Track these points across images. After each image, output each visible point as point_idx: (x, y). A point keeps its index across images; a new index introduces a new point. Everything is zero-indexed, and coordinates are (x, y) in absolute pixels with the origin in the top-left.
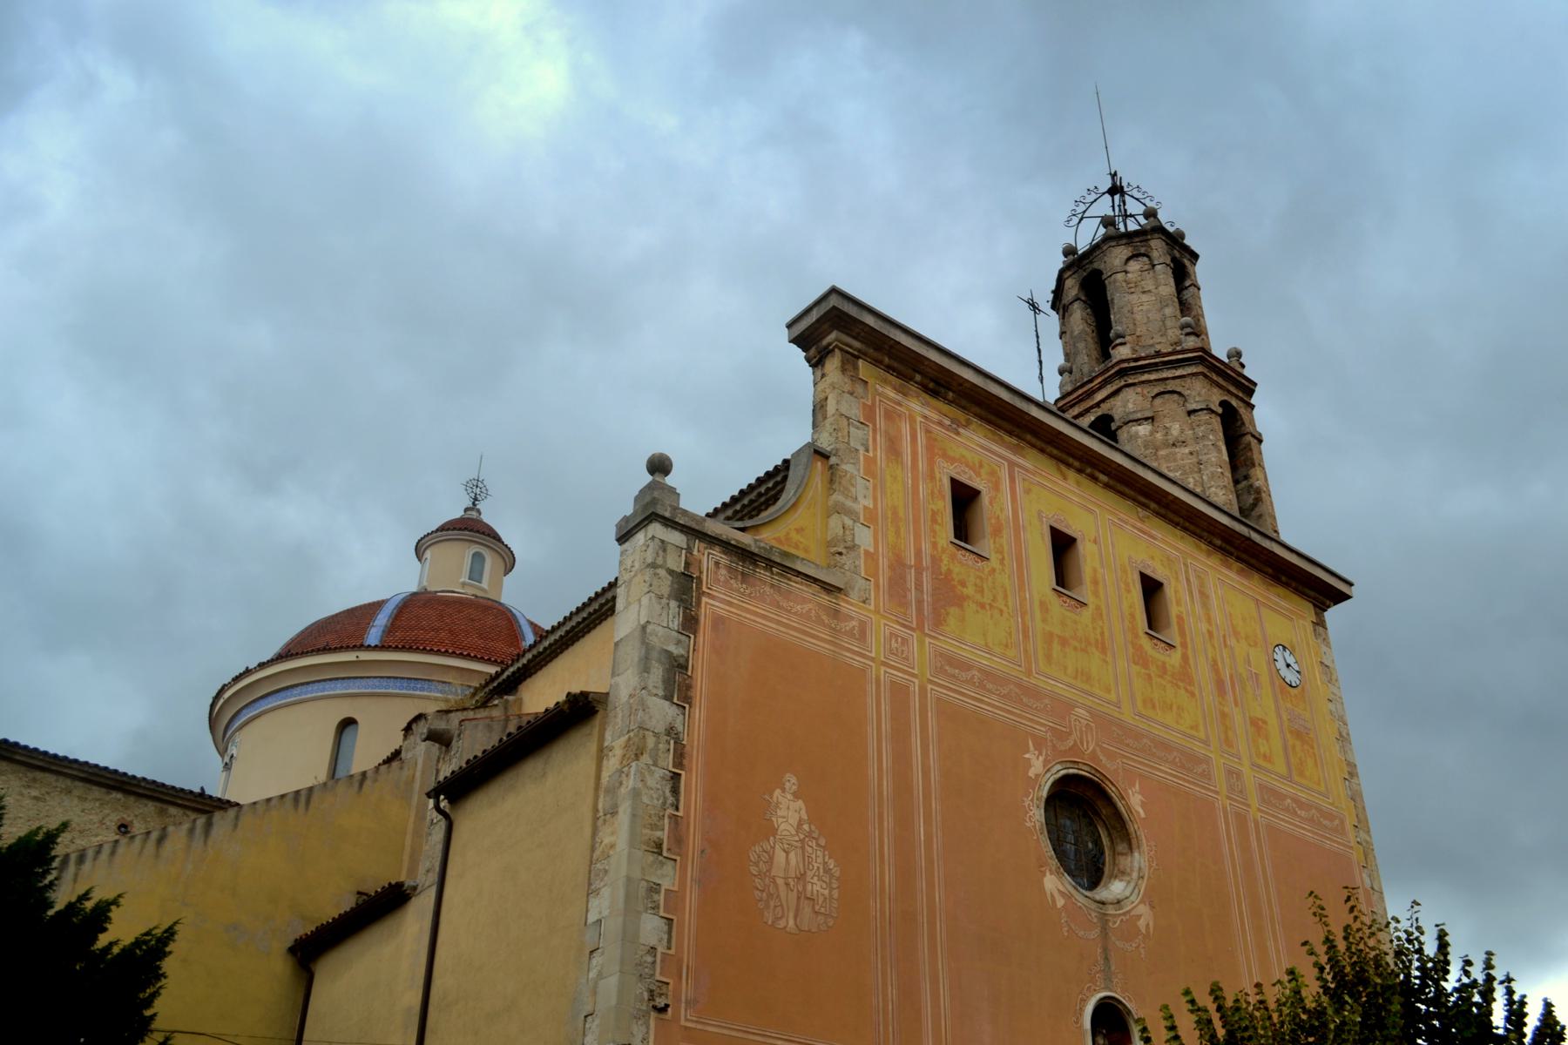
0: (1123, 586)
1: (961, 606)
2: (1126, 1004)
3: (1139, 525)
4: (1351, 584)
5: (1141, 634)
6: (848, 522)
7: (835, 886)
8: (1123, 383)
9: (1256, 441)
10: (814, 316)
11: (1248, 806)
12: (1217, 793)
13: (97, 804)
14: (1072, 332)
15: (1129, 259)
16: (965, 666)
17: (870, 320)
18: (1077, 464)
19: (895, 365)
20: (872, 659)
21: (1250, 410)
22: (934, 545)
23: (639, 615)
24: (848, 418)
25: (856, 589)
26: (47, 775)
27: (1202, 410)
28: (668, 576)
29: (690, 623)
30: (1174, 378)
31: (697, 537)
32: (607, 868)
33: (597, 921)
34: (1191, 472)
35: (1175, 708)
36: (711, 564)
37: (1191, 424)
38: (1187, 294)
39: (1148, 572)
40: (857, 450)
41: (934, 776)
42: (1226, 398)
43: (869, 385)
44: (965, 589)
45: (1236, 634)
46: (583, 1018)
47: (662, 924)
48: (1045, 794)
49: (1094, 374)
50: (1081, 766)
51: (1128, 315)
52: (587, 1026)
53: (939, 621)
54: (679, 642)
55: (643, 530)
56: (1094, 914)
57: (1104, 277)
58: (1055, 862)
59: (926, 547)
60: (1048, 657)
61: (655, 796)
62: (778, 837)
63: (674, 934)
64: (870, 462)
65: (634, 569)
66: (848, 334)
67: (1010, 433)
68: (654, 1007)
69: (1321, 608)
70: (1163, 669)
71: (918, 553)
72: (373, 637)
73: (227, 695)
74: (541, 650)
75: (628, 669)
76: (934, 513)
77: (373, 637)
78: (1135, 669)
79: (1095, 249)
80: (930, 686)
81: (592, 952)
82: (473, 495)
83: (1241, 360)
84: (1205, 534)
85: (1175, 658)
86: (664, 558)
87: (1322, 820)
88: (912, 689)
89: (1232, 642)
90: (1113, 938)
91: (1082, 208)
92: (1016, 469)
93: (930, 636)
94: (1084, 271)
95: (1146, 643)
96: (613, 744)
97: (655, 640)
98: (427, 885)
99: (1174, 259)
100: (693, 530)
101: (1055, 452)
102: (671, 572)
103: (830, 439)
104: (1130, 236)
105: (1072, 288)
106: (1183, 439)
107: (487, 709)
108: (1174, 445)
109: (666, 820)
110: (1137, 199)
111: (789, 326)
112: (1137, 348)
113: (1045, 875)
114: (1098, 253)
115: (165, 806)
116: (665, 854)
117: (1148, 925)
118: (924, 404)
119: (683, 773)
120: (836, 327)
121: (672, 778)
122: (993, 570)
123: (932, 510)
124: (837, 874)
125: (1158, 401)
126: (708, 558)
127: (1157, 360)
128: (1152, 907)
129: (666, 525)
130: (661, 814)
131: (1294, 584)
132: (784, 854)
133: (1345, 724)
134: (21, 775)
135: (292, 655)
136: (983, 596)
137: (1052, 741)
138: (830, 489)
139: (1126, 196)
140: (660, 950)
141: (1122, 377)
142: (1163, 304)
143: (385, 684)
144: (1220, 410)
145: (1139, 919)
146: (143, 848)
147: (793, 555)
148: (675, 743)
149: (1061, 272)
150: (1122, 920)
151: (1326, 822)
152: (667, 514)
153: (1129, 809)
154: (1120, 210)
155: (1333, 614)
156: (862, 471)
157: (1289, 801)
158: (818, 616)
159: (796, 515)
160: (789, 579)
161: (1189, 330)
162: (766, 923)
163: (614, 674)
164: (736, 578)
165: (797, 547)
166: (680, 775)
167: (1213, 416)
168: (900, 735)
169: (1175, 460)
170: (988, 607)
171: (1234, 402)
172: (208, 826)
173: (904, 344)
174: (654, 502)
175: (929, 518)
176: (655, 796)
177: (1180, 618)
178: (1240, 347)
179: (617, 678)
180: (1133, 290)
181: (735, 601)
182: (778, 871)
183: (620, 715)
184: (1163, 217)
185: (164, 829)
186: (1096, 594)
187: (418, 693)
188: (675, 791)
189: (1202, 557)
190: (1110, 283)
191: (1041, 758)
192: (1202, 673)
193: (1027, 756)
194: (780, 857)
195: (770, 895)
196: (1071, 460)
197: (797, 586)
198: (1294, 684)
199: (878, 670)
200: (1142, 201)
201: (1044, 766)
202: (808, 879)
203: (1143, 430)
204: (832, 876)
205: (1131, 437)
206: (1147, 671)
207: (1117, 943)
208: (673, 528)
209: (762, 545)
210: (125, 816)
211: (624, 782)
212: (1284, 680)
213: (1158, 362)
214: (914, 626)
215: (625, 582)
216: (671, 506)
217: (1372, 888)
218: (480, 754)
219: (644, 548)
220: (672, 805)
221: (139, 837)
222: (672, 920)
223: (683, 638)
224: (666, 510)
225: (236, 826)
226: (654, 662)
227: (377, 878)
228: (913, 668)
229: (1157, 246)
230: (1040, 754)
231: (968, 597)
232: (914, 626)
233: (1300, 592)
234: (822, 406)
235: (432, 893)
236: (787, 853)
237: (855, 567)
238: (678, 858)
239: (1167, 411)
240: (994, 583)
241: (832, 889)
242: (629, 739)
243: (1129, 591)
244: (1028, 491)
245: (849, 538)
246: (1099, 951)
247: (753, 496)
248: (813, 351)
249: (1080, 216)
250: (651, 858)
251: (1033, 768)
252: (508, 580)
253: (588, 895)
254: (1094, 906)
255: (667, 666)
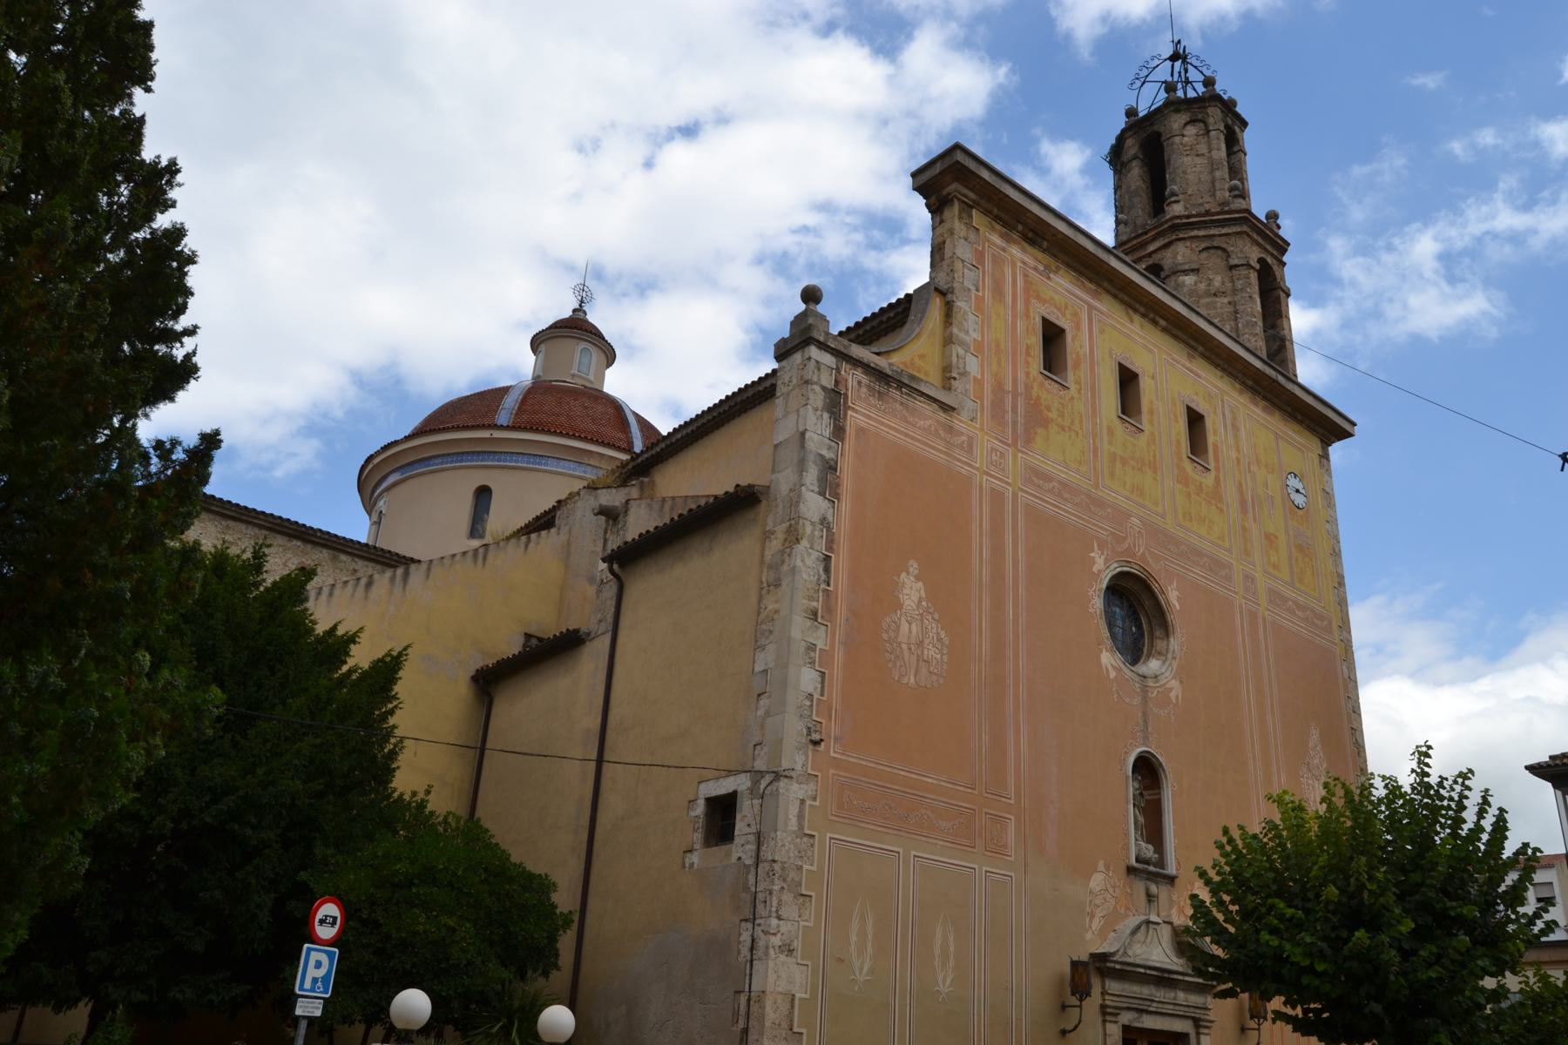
0: (1172, 417)
1: (1046, 427)
2: (1159, 758)
3: (1188, 365)
4: (1354, 424)
5: (1184, 457)
6: (961, 352)
7: (945, 652)
8: (1174, 237)
9: (1284, 295)
10: (938, 168)
11: (1259, 605)
12: (1236, 593)
13: (281, 549)
14: (1129, 187)
15: (1186, 124)
16: (1047, 478)
17: (985, 175)
18: (1142, 309)
19: (1003, 215)
20: (977, 469)
21: (1281, 267)
22: (1028, 374)
23: (797, 423)
24: (963, 261)
25: (966, 408)
26: (238, 523)
27: (1242, 265)
28: (821, 391)
29: (839, 432)
30: (1220, 235)
31: (844, 359)
32: (772, 629)
33: (764, 671)
34: (1229, 320)
35: (1207, 522)
36: (855, 383)
37: (1232, 277)
38: (1234, 159)
39: (1193, 406)
40: (969, 290)
41: (1022, 566)
42: (1263, 255)
43: (981, 232)
44: (1049, 414)
45: (1258, 462)
46: (752, 746)
47: (815, 675)
48: (1104, 586)
49: (1148, 227)
50: (1134, 566)
51: (1182, 175)
52: (756, 753)
53: (1029, 440)
54: (830, 448)
55: (800, 351)
56: (1137, 685)
57: (1163, 139)
58: (1109, 642)
59: (1021, 375)
60: (1112, 474)
61: (812, 573)
62: (903, 611)
63: (826, 684)
64: (980, 300)
65: (791, 384)
66: (967, 187)
67: (1091, 280)
68: (811, 741)
69: (1326, 443)
70: (1200, 487)
71: (1015, 380)
72: (503, 418)
73: (376, 461)
74: (673, 441)
75: (787, 468)
76: (1028, 347)
77: (503, 418)
78: (1179, 487)
79: (1153, 115)
80: (1020, 494)
81: (759, 695)
82: (580, 298)
83: (1278, 222)
84: (1240, 375)
85: (1209, 480)
86: (819, 376)
87: (1315, 620)
88: (1006, 494)
89: (1254, 468)
90: (1151, 706)
91: (1145, 72)
92: (1094, 311)
93: (1023, 452)
94: (1145, 132)
95: (1188, 466)
96: (776, 529)
97: (812, 445)
98: (600, 632)
99: (1227, 126)
100: (842, 353)
101: (1126, 298)
102: (824, 388)
103: (947, 278)
104: (1188, 102)
105: (1132, 148)
106: (1224, 290)
107: (628, 488)
108: (1215, 295)
109: (821, 594)
110: (1195, 67)
111: (914, 175)
112: (1188, 206)
113: (1101, 652)
114: (1159, 116)
115: (336, 553)
116: (819, 620)
117: (1177, 697)
118: (1024, 250)
119: (833, 555)
120: (957, 179)
121: (825, 559)
122: (1072, 398)
123: (1027, 344)
124: (947, 643)
125: (1205, 254)
126: (854, 378)
127: (1206, 218)
128: (1181, 682)
129: (820, 348)
130: (816, 588)
131: (1307, 422)
132: (908, 625)
133: (1339, 542)
134: (216, 523)
135: (426, 431)
136: (1064, 421)
137: (1111, 544)
138: (946, 322)
139: (1189, 67)
140: (816, 696)
141: (1174, 231)
142: (1213, 166)
143: (538, 460)
144: (1258, 267)
145: (1171, 692)
146: (354, 591)
147: (919, 378)
148: (827, 530)
149: (1123, 131)
150: (1158, 692)
151: (1318, 622)
152: (822, 339)
153: (1168, 602)
154: (1180, 76)
155: (1337, 450)
156: (973, 308)
157: (1290, 603)
158: (936, 430)
159: (919, 344)
160: (915, 399)
161: (1237, 193)
162: (893, 679)
163: (773, 471)
164: (874, 396)
165: (919, 371)
166: (831, 557)
167: (1252, 271)
168: (997, 531)
169: (1215, 308)
170: (1067, 429)
171: (1269, 260)
172: (406, 575)
173: (1013, 197)
174: (809, 328)
175: (1024, 351)
176: (812, 573)
177: (1215, 446)
178: (1278, 210)
179: (777, 475)
180: (1188, 153)
181: (874, 416)
182: (903, 638)
183: (781, 506)
184: (1218, 88)
185: (371, 576)
186: (1151, 422)
187: (543, 467)
188: (827, 570)
189: (1235, 394)
190: (1168, 144)
191: (1103, 557)
192: (1230, 493)
193: (1092, 555)
194: (905, 627)
195: (897, 657)
196: (1138, 306)
197: (921, 405)
198: (1301, 507)
199: (981, 478)
200: (1200, 69)
201: (1105, 564)
202: (926, 646)
203: (1189, 280)
204: (943, 644)
205: (1178, 285)
206: (1188, 490)
207: (1154, 709)
208: (825, 350)
209: (895, 368)
210: (304, 560)
211: (787, 561)
212: (1293, 502)
213: (1205, 220)
214: (1010, 442)
215: (783, 394)
216: (825, 332)
217: (1350, 678)
218: (652, 530)
219: (801, 367)
220: (825, 581)
221: (351, 582)
222: (824, 673)
223: (833, 444)
224: (820, 335)
225: (428, 576)
226: (811, 463)
227: (549, 625)
228: (1008, 478)
229: (1214, 115)
230: (1102, 554)
231: (1052, 420)
232: (1010, 442)
233: (1313, 430)
234: (940, 249)
235: (607, 639)
236: (910, 624)
237: (966, 390)
238: (829, 624)
239: (1211, 265)
240: (1072, 409)
241: (942, 655)
242: (791, 525)
243: (1177, 421)
244: (1102, 332)
245: (961, 366)
246: (1140, 714)
247: (875, 323)
248: (933, 198)
249: (1142, 80)
250: (809, 623)
251: (1096, 565)
252: (610, 374)
253: (755, 649)
254: (1137, 679)
255: (821, 467)
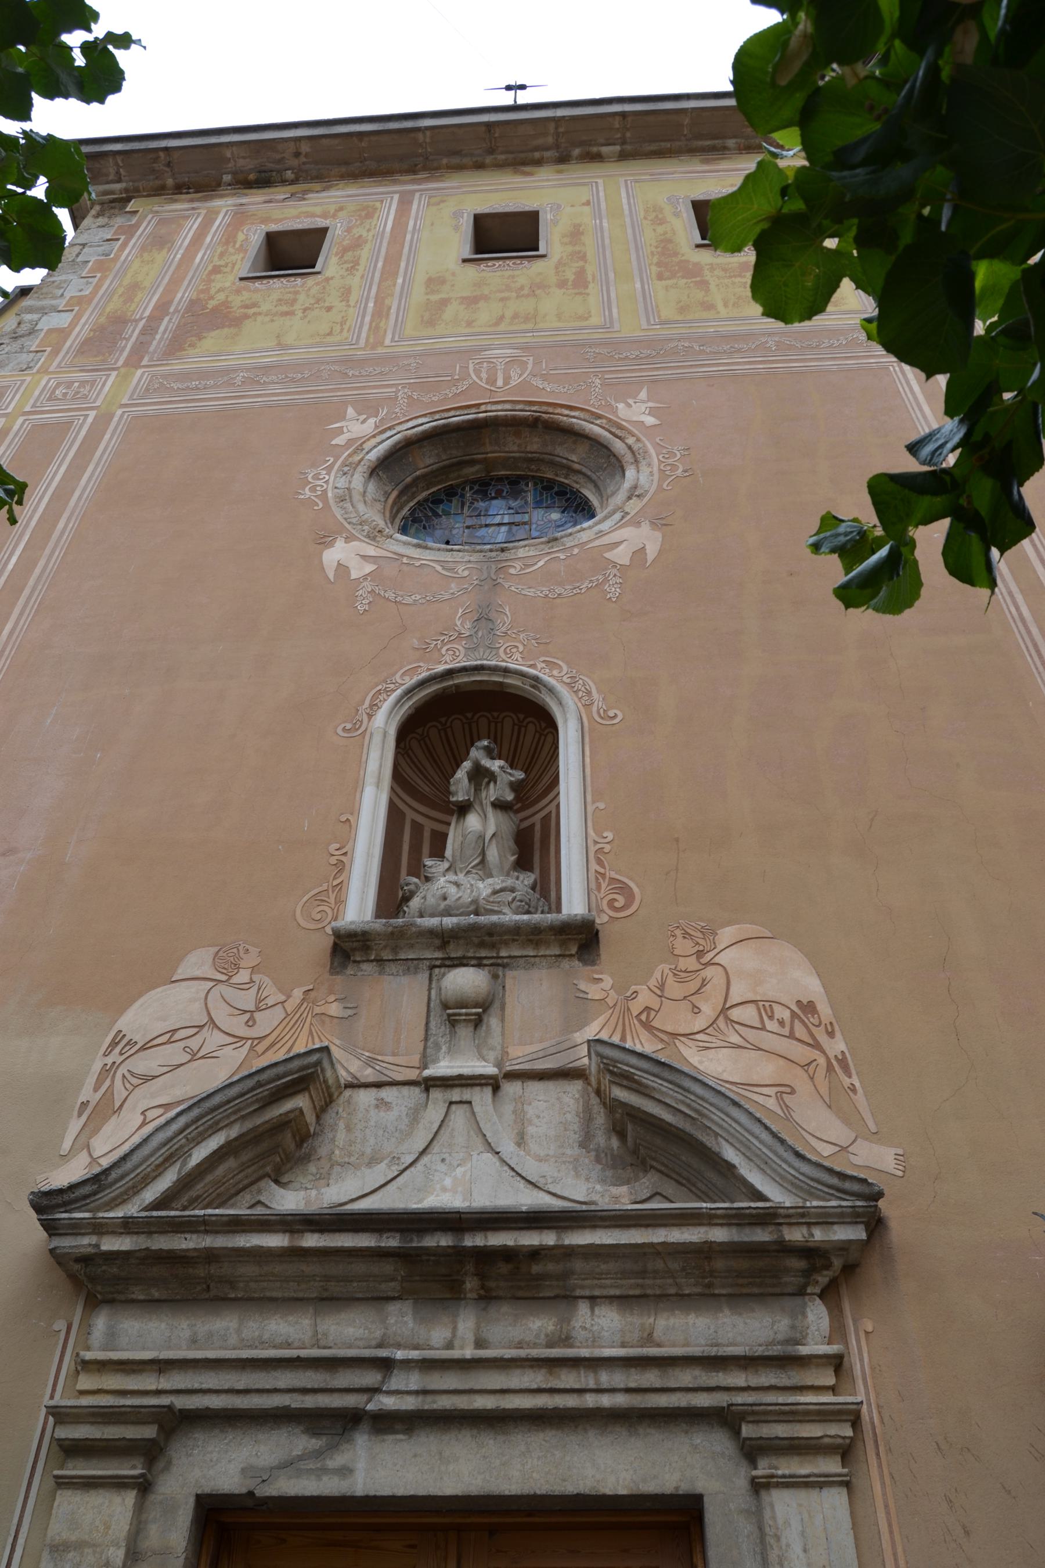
117: (365, 557)
